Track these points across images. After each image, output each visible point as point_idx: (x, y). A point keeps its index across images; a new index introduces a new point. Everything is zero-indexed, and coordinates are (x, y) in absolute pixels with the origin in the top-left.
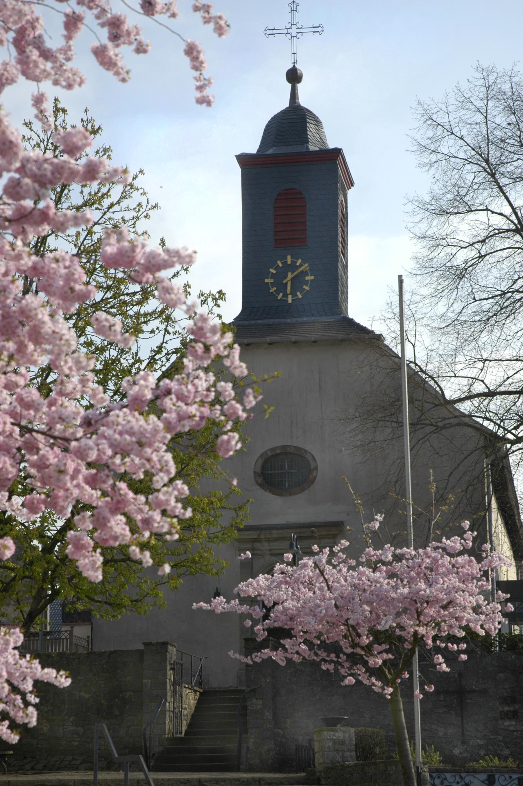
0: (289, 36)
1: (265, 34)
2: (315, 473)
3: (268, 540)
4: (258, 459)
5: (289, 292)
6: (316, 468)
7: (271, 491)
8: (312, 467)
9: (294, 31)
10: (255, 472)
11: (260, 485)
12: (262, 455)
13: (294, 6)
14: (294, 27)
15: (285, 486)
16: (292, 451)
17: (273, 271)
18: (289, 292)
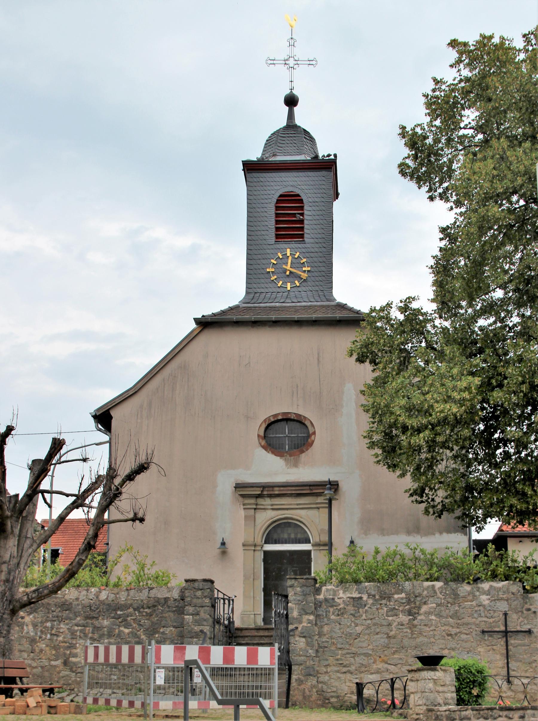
0: (287, 66)
1: (267, 63)
2: (313, 437)
3: (271, 496)
4: (262, 423)
5: (290, 258)
6: (314, 433)
7: (273, 453)
8: (311, 432)
9: (291, 62)
10: (259, 436)
11: (263, 447)
12: (265, 421)
13: (292, 42)
14: (291, 65)
15: (286, 449)
16: (292, 418)
17: (273, 261)
18: (290, 258)
